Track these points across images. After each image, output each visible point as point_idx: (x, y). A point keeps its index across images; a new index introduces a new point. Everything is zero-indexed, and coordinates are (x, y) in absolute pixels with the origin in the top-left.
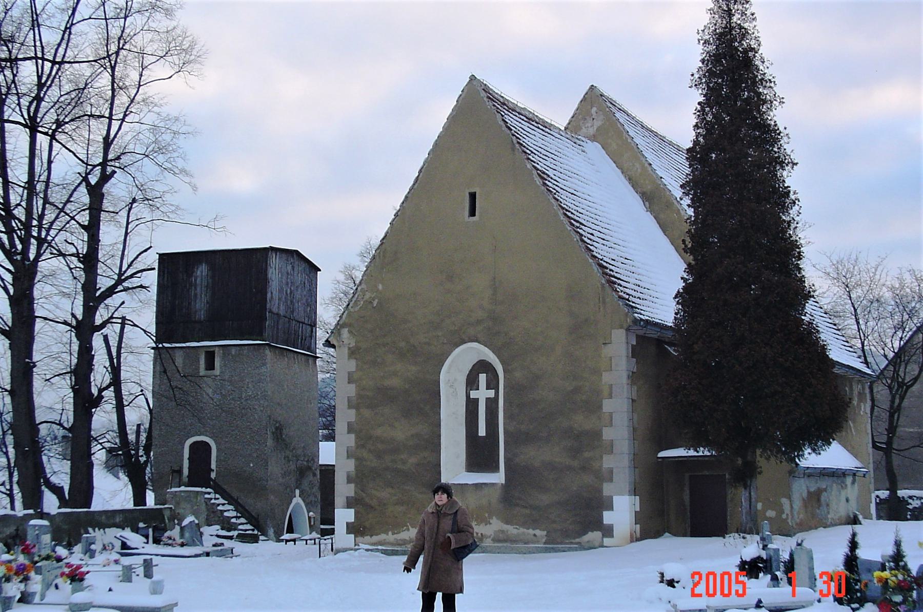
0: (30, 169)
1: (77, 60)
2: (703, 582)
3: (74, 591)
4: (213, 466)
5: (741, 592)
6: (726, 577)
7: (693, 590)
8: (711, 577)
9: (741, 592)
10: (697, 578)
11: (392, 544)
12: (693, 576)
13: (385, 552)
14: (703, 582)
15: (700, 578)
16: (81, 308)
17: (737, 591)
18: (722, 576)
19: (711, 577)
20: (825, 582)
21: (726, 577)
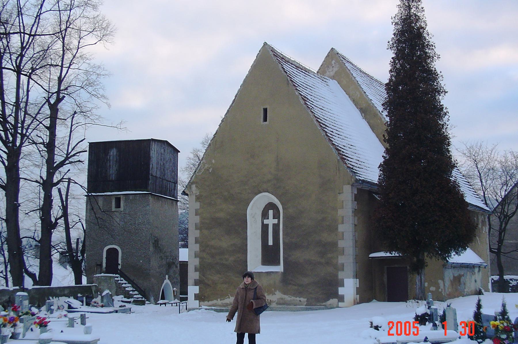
2: (395, 327)
5: (416, 333)
6: (408, 324)
7: (389, 332)
8: (399, 324)
9: (416, 333)
10: (391, 325)
12: (389, 324)
14: (395, 327)
15: (393, 325)
18: (405, 323)
19: (399, 324)
21: (408, 324)
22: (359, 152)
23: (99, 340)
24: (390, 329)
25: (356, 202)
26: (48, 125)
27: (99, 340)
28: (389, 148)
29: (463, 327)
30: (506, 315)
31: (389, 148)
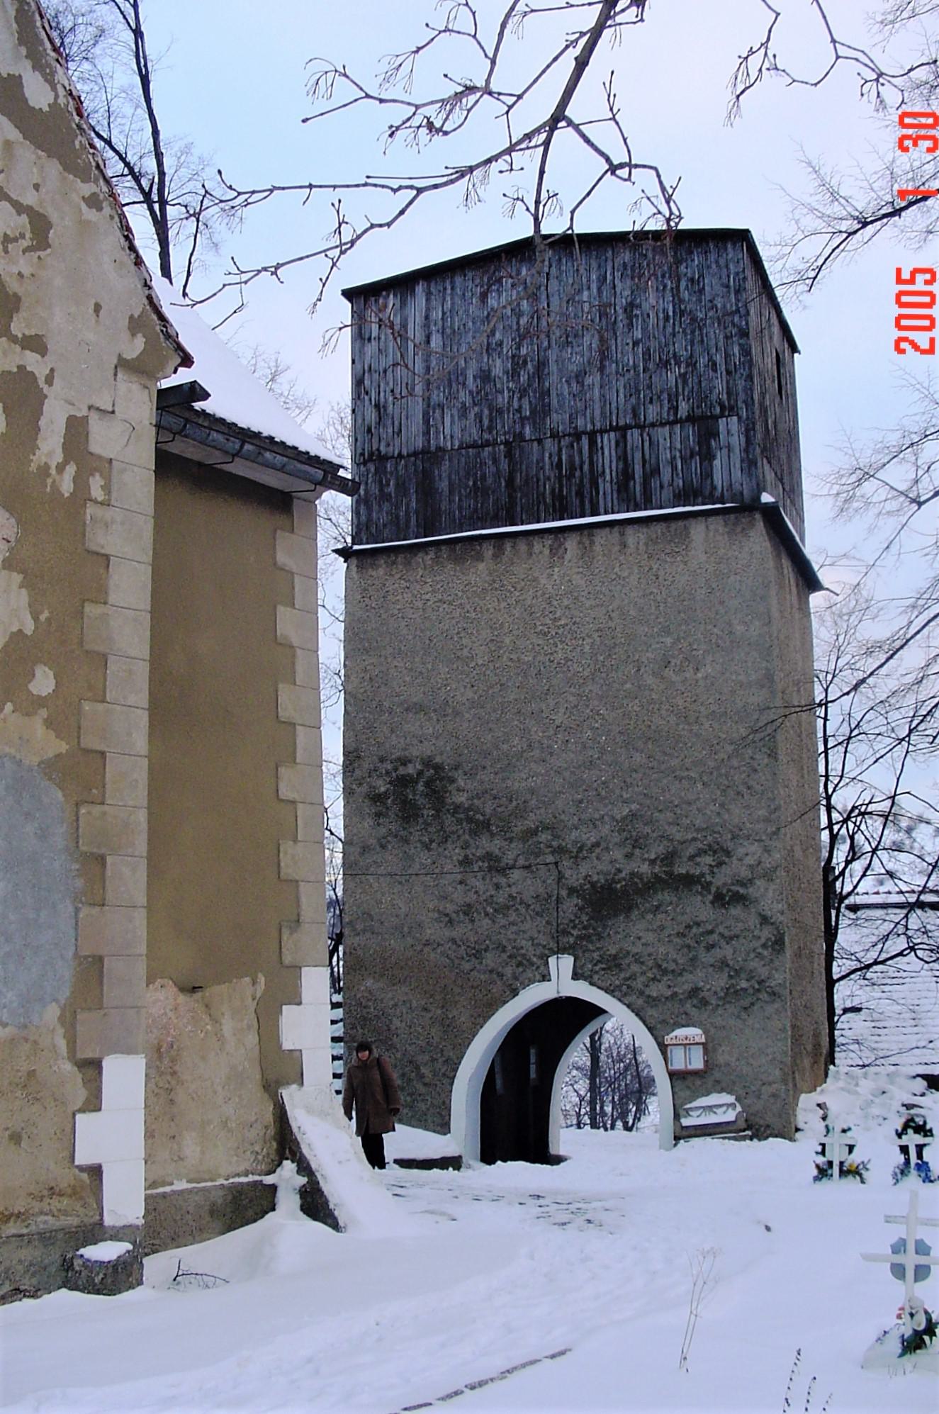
0: (75, 1047)
1: (359, 232)
2: (911, 335)
3: (932, 1135)
4: (333, 579)
5: (928, 276)
6: (904, 299)
7: (924, 352)
8: (904, 322)
9: (928, 276)
10: (903, 345)
11: (761, 404)
12: (902, 351)
13: (735, 1139)
14: (911, 335)
15: (905, 339)
16: (175, 451)
17: (927, 282)
18: (902, 305)
19: (904, 322)
20: (915, 144)
21: (904, 299)
22: (923, 1022)
23: (863, 1182)
24: (915, 346)
25: (287, 1045)
26: (247, 979)
27: (863, 1182)
28: (198, 405)
29: (915, 144)
30: (449, 559)
31: (198, 405)
